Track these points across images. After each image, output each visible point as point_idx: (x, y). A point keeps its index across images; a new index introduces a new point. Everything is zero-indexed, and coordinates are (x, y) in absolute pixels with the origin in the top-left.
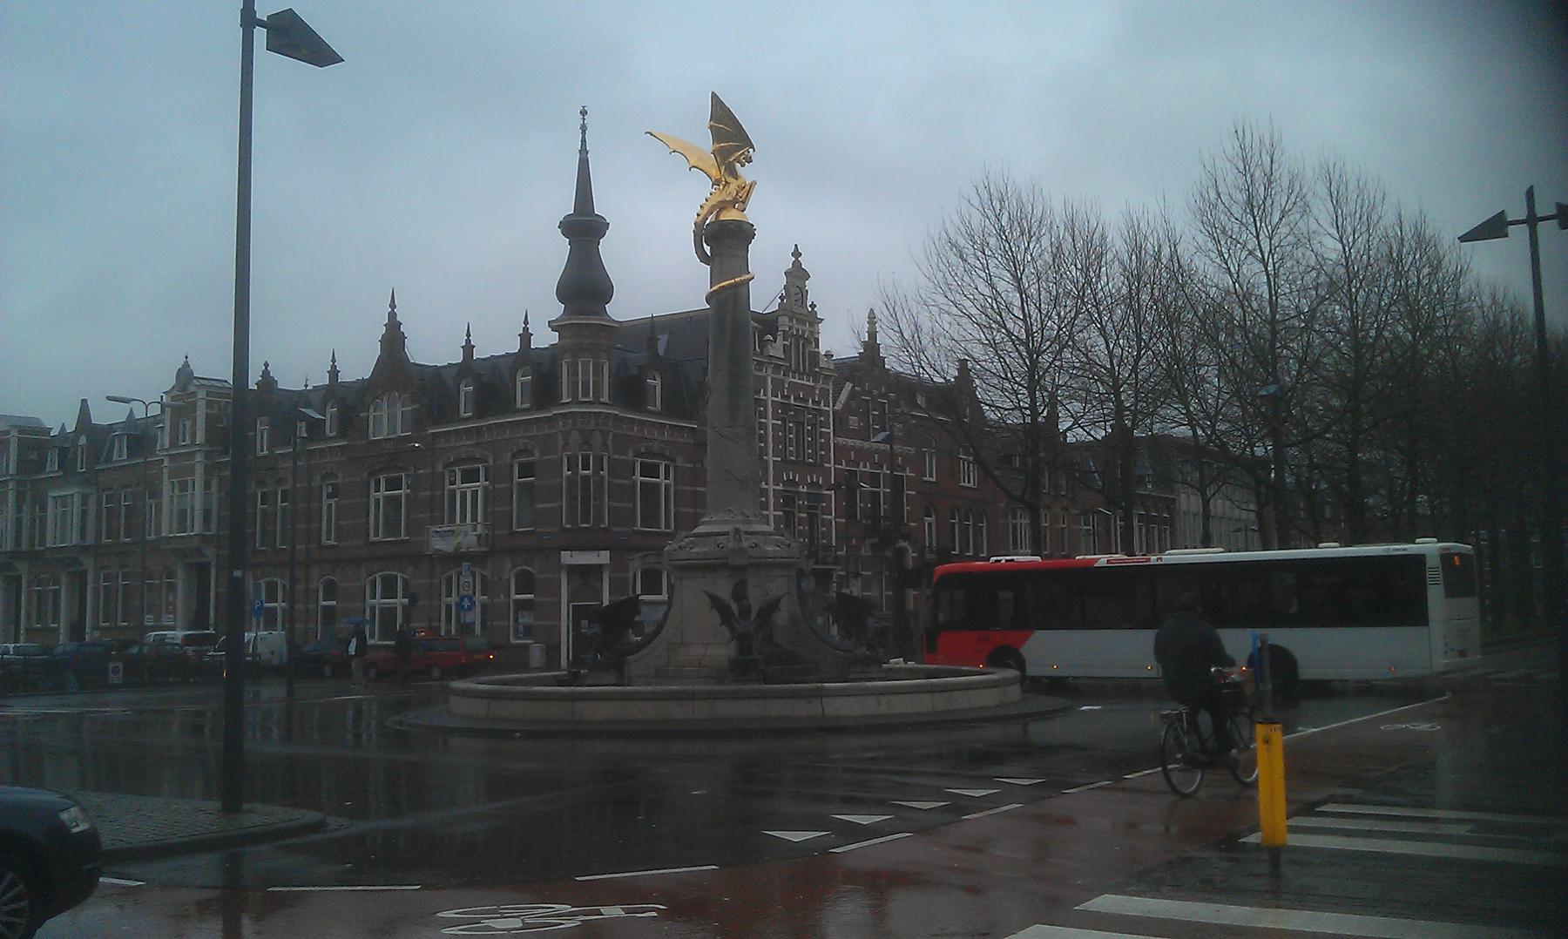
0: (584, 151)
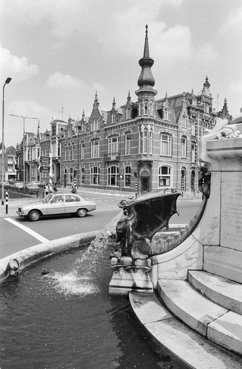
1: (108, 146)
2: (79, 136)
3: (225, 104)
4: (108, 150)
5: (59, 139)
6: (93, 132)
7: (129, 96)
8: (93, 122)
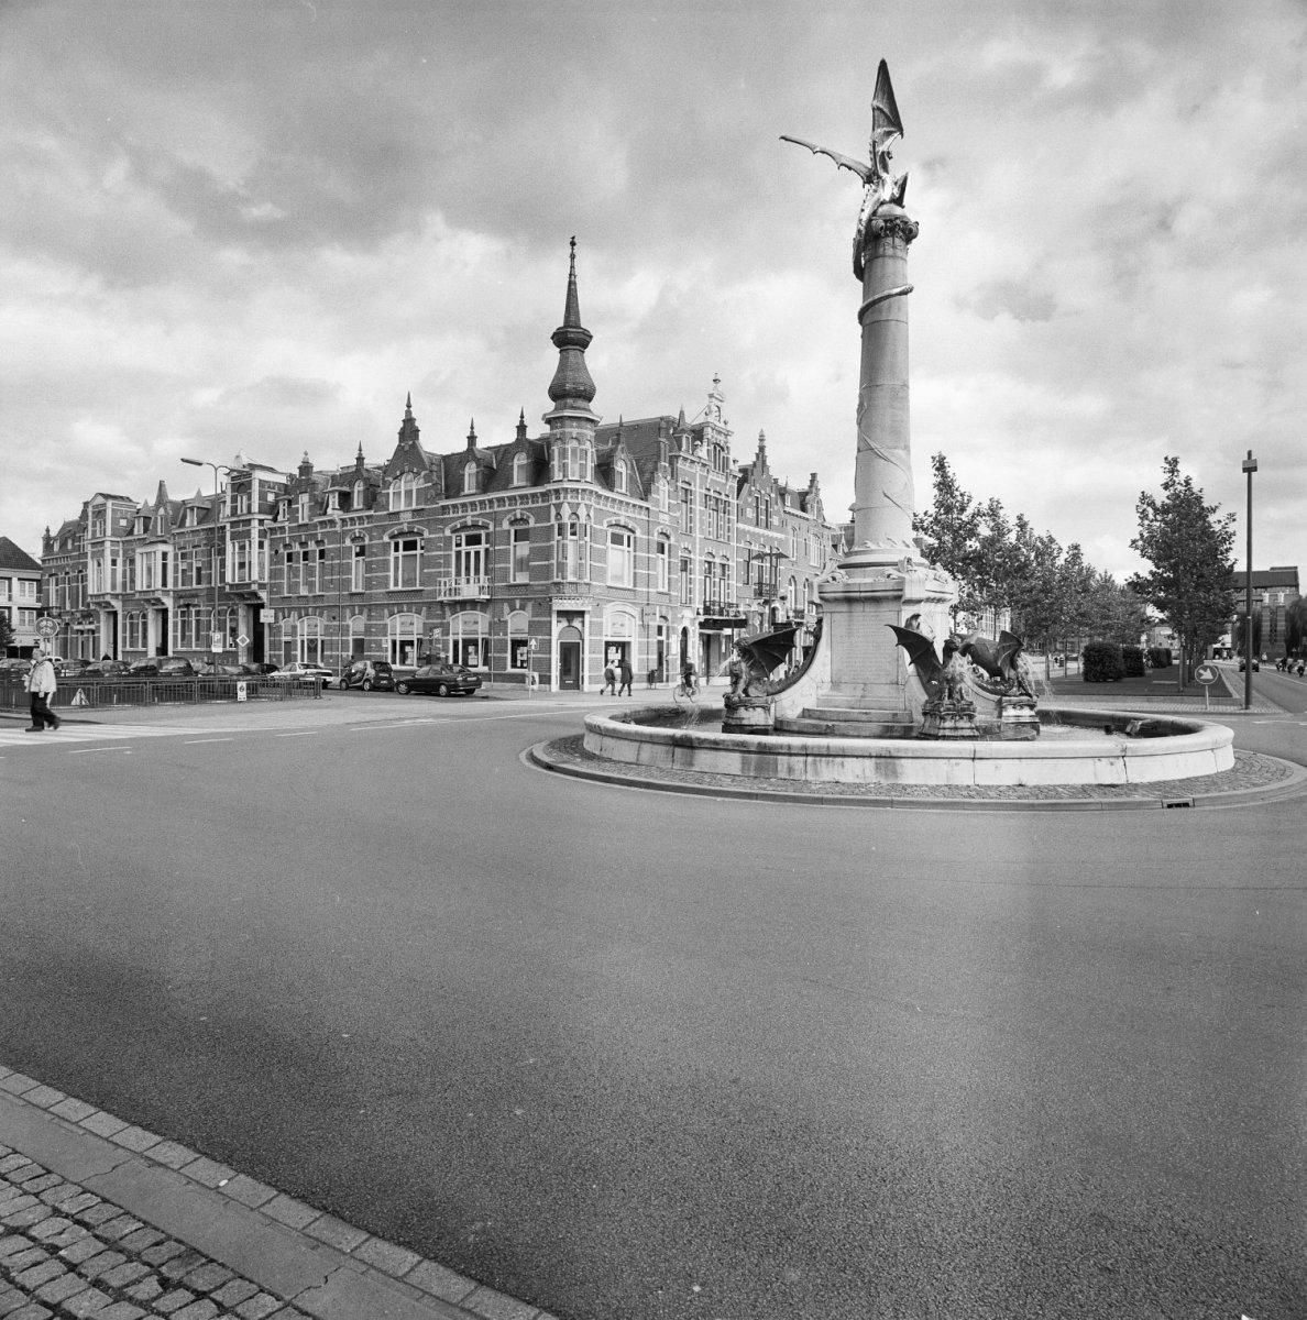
0: (572, 285)
2: (343, 520)
3: (762, 449)
6: (398, 513)
7: (522, 422)
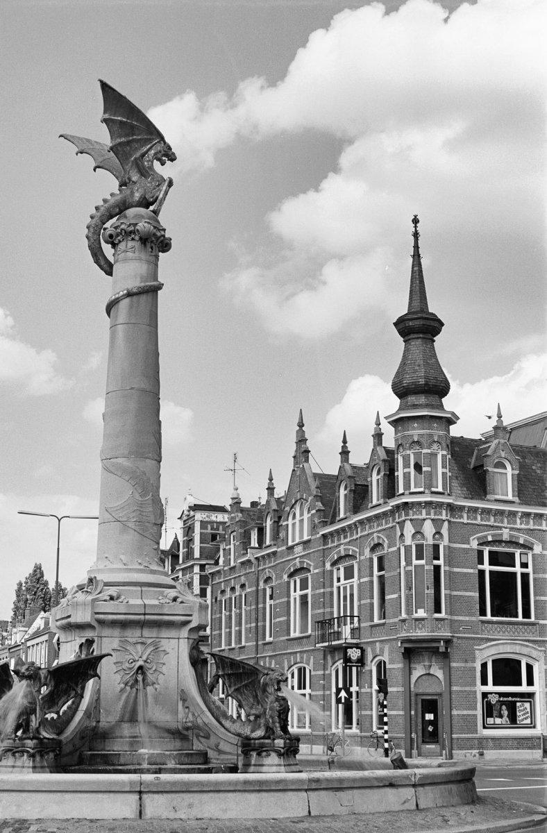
1: (332, 594)
4: (332, 607)
5: (203, 573)
8: (295, 514)
